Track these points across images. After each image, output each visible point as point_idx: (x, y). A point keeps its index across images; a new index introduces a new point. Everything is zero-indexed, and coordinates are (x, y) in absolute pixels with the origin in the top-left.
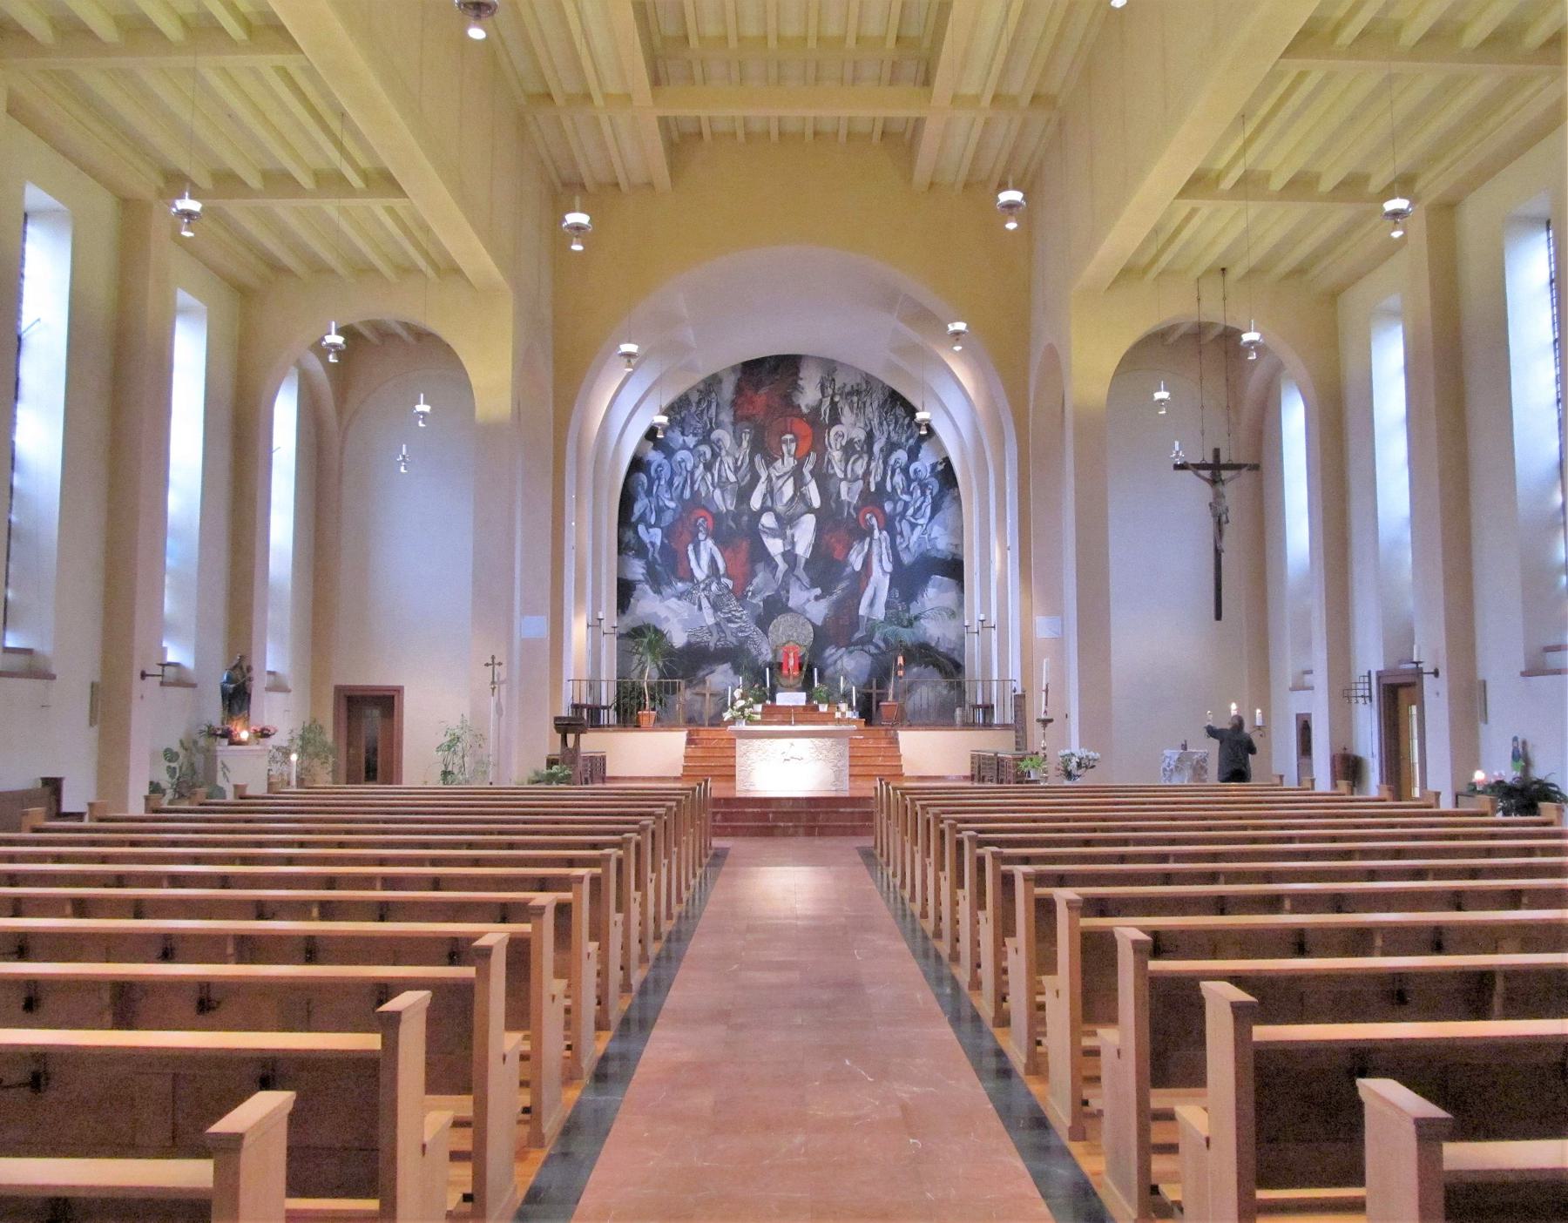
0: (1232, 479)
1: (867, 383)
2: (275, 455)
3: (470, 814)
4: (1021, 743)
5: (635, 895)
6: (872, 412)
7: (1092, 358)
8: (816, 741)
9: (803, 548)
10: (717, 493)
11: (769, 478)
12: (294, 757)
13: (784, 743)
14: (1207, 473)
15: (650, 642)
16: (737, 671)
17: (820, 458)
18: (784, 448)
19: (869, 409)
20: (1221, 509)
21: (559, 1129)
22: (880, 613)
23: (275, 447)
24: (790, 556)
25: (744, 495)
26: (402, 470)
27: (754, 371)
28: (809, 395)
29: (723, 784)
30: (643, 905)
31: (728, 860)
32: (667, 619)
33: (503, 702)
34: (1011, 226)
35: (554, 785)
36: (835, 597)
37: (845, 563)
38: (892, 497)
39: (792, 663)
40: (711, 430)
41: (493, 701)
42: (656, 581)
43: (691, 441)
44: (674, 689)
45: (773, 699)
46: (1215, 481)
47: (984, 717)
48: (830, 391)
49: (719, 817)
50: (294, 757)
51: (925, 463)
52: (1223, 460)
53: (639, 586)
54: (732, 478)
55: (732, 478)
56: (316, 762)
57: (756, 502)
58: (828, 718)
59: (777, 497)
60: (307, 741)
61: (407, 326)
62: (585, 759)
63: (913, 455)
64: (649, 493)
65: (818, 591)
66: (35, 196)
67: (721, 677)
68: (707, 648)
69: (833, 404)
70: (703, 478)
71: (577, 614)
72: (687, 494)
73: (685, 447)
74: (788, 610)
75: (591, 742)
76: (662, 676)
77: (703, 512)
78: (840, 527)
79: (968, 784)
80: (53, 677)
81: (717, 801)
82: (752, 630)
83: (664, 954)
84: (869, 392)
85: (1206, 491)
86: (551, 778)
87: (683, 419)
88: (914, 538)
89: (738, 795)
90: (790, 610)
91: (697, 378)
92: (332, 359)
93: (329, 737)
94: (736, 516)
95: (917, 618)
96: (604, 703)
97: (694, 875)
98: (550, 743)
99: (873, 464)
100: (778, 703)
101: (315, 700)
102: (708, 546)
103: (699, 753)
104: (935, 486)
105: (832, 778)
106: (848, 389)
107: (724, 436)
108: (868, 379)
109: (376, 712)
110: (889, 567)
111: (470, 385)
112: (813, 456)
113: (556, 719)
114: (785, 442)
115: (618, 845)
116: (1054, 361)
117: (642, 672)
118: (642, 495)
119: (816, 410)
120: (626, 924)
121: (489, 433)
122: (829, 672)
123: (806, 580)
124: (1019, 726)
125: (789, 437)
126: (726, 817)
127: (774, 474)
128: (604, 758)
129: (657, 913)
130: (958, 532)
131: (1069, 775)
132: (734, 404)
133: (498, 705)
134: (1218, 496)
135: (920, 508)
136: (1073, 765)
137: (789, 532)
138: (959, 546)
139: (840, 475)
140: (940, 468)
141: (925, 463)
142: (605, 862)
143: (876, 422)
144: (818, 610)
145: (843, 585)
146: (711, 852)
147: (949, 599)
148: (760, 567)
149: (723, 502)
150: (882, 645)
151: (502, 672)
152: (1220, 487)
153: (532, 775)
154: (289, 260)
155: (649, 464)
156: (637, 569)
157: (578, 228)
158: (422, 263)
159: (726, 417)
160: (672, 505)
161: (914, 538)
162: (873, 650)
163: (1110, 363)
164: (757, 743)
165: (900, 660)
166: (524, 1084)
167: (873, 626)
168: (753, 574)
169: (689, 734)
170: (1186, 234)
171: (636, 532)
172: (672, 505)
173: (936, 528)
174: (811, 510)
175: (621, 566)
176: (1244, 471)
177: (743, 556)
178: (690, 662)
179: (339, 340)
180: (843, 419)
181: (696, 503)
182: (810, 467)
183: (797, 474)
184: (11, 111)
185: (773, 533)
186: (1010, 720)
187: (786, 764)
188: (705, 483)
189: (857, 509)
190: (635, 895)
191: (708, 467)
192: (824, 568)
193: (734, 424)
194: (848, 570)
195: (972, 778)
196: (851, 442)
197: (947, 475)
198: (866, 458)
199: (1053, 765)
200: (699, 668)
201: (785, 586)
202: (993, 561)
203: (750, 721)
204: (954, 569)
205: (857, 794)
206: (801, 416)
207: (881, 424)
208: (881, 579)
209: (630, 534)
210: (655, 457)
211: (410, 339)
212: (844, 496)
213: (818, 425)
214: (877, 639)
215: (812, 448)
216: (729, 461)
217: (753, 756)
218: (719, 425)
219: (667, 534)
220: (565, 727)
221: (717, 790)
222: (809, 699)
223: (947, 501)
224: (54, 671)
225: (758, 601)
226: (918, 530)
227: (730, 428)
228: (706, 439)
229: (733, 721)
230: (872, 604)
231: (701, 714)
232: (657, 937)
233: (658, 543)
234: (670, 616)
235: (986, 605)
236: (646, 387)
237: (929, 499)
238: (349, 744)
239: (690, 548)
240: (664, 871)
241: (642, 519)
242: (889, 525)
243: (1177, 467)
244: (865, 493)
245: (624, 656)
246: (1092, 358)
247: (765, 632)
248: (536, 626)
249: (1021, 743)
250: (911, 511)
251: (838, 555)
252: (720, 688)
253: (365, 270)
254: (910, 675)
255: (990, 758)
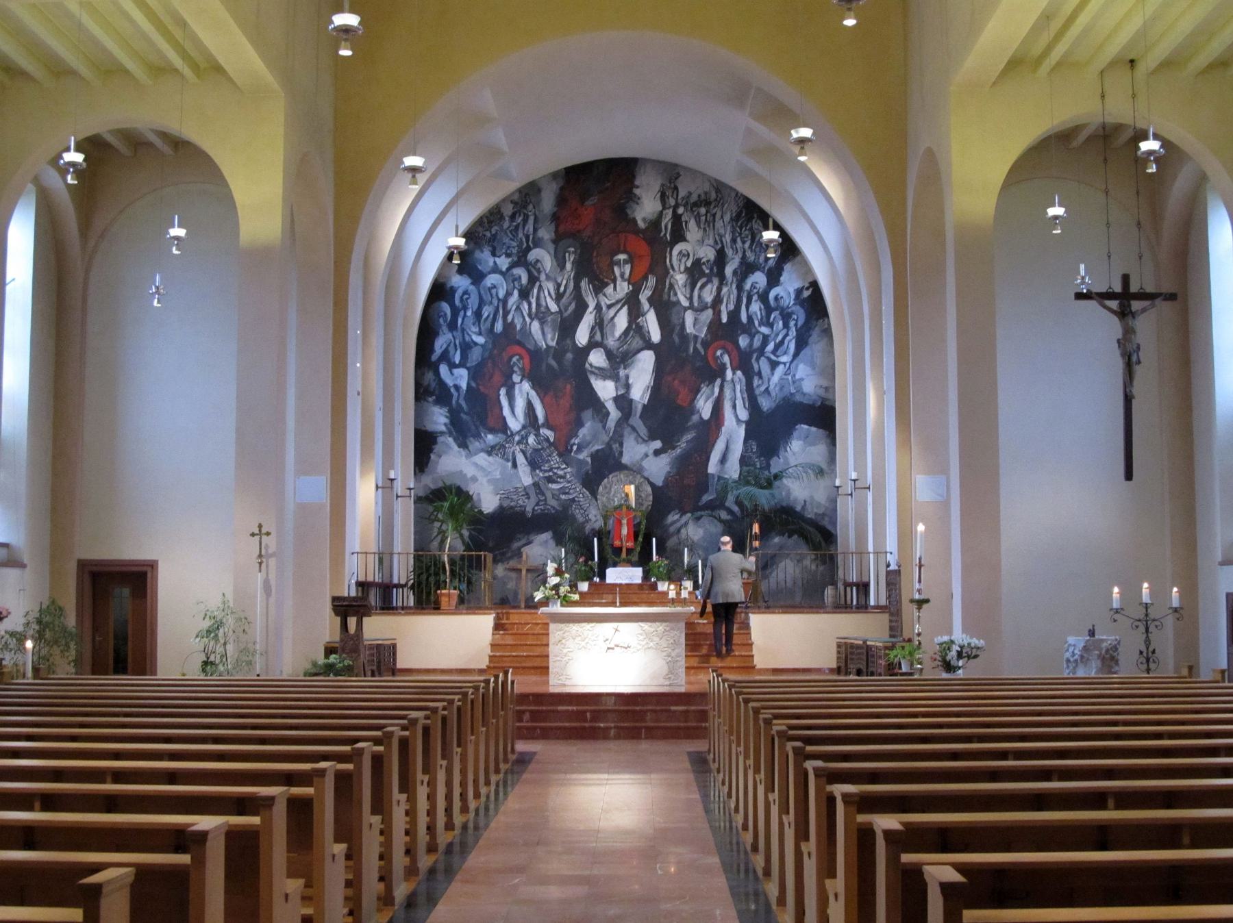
0: (1144, 310)
1: (718, 191)
2: (8, 288)
3: (247, 713)
4: (895, 629)
5: (398, 797)
6: (723, 226)
7: (977, 162)
8: (646, 626)
9: (640, 391)
10: (535, 326)
11: (598, 307)
12: (29, 644)
13: (608, 627)
14: (1114, 304)
15: (452, 506)
16: (559, 540)
17: (660, 282)
18: (616, 269)
19: (719, 224)
20: (1129, 347)
22: (733, 470)
23: (8, 279)
24: (623, 401)
25: (567, 327)
26: (155, 303)
27: (578, 178)
28: (647, 207)
29: (534, 678)
30: (411, 813)
31: (531, 767)
32: (474, 479)
33: (272, 576)
34: (850, 22)
35: (332, 677)
36: (678, 451)
37: (692, 410)
38: (749, 329)
39: (625, 531)
40: (529, 249)
41: (260, 577)
42: (462, 433)
43: (503, 262)
44: (478, 564)
45: (603, 576)
46: (1124, 314)
47: (855, 598)
48: (672, 202)
49: (527, 716)
50: (29, 644)
51: (789, 286)
52: (1134, 288)
53: (441, 439)
54: (553, 307)
55: (553, 307)
56: (56, 650)
57: (582, 336)
58: (663, 599)
59: (607, 330)
60: (46, 625)
61: (164, 135)
62: (371, 647)
63: (774, 278)
64: (452, 326)
65: (658, 444)
67: (542, 551)
68: (523, 513)
69: (677, 218)
70: (518, 308)
71: (363, 473)
72: (499, 327)
73: (495, 269)
74: (621, 467)
75: (376, 628)
76: (468, 548)
77: (517, 349)
78: (683, 365)
79: (835, 677)
81: (523, 698)
82: (578, 492)
84: (719, 201)
85: (1114, 327)
86: (329, 669)
87: (494, 237)
88: (776, 378)
89: (553, 690)
90: (622, 467)
91: (510, 187)
92: (70, 179)
93: (71, 621)
94: (558, 353)
95: (777, 477)
96: (395, 581)
97: (488, 783)
98: (327, 627)
99: (725, 290)
100: (609, 580)
101: (55, 575)
102: (524, 390)
103: (509, 640)
104: (800, 315)
105: (665, 670)
106: (694, 198)
107: (543, 256)
108: (719, 187)
109: (126, 592)
110: (744, 415)
111: (234, 203)
112: (652, 281)
113: (335, 599)
114: (618, 263)
115: (377, 741)
116: (934, 174)
117: (443, 542)
118: (445, 328)
119: (655, 224)
120: (386, 832)
121: (259, 257)
122: (671, 543)
123: (643, 431)
124: (893, 609)
125: (622, 257)
126: (535, 716)
127: (605, 302)
128: (394, 646)
130: (828, 372)
131: (948, 667)
132: (555, 218)
133: (266, 583)
134: (1128, 332)
135: (782, 342)
136: (953, 654)
137: (622, 373)
138: (830, 389)
139: (685, 303)
140: (806, 294)
141: (789, 286)
142: (395, 766)
143: (728, 238)
144: (658, 468)
145: (689, 436)
146: (512, 757)
147: (817, 453)
148: (587, 415)
149: (542, 336)
150: (736, 509)
151: (271, 542)
152: (1130, 321)
153: (308, 666)
154: (22, 60)
155: (453, 290)
156: (439, 419)
157: (346, 30)
158: (177, 61)
159: (546, 233)
160: (480, 340)
161: (776, 378)
162: (724, 515)
163: (998, 171)
164: (575, 628)
165: (756, 528)
167: (725, 486)
168: (580, 424)
169: (498, 618)
170: (1083, 20)
171: (437, 373)
172: (480, 340)
173: (801, 366)
174: (649, 345)
175: (419, 415)
176: (1158, 301)
177: (566, 402)
178: (502, 531)
179: (78, 158)
180: (688, 236)
181: (509, 338)
182: (648, 293)
183: (632, 302)
185: (603, 374)
186: (883, 602)
187: (611, 653)
188: (519, 314)
189: (705, 344)
190: (398, 797)
191: (524, 294)
192: (665, 415)
193: (555, 242)
194: (695, 418)
195: (838, 671)
196: (697, 263)
197: (814, 303)
198: (716, 282)
199: (928, 654)
200: (511, 539)
201: (618, 437)
202: (867, 407)
203: (567, 602)
204: (822, 416)
205: (694, 689)
206: (636, 231)
207: (734, 241)
208: (734, 431)
209: (429, 376)
210: (460, 282)
211: (167, 150)
212: (690, 329)
213: (655, 244)
214: (730, 502)
215: (651, 270)
216: (549, 286)
217: (571, 644)
218: (538, 243)
219: (475, 374)
220: (345, 608)
221: (523, 684)
222: (646, 576)
223: (815, 335)
225: (584, 456)
226: (780, 370)
227: (551, 247)
228: (521, 260)
229: (545, 602)
230: (723, 460)
231: (516, 594)
232: (432, 848)
233: (464, 385)
234: (479, 475)
235: (860, 465)
236: (447, 198)
237: (793, 332)
238: (95, 629)
239: (503, 392)
240: (441, 776)
241: (445, 357)
242: (744, 363)
243: (1079, 296)
244: (715, 324)
245: (423, 522)
246: (977, 162)
247: (594, 493)
248: (316, 488)
249: (895, 629)
250: (771, 347)
251: (682, 399)
252: (536, 562)
253: (112, 71)
254: (805, 547)
255: (858, 647)
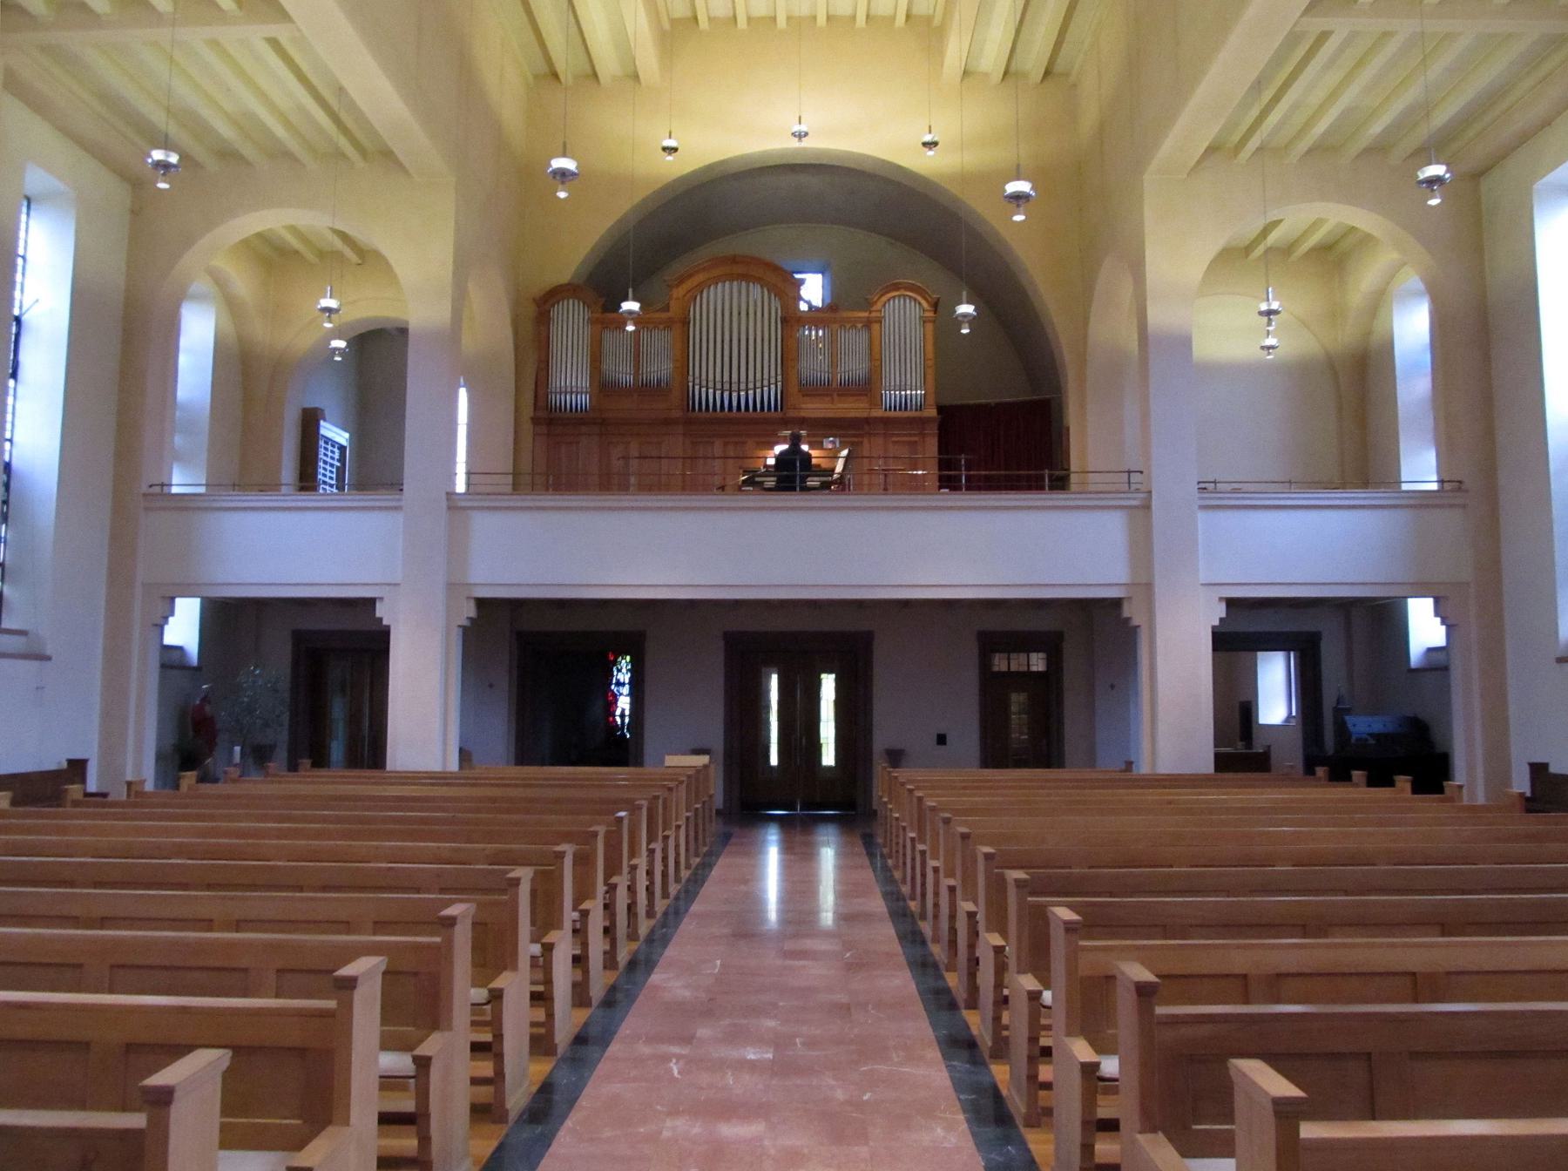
21: (571, 1037)
66: (36, 179)
80: (49, 658)
83: (671, 910)
129: (631, 908)
166: (477, 1048)
184: (6, 86)
224: (48, 653)
